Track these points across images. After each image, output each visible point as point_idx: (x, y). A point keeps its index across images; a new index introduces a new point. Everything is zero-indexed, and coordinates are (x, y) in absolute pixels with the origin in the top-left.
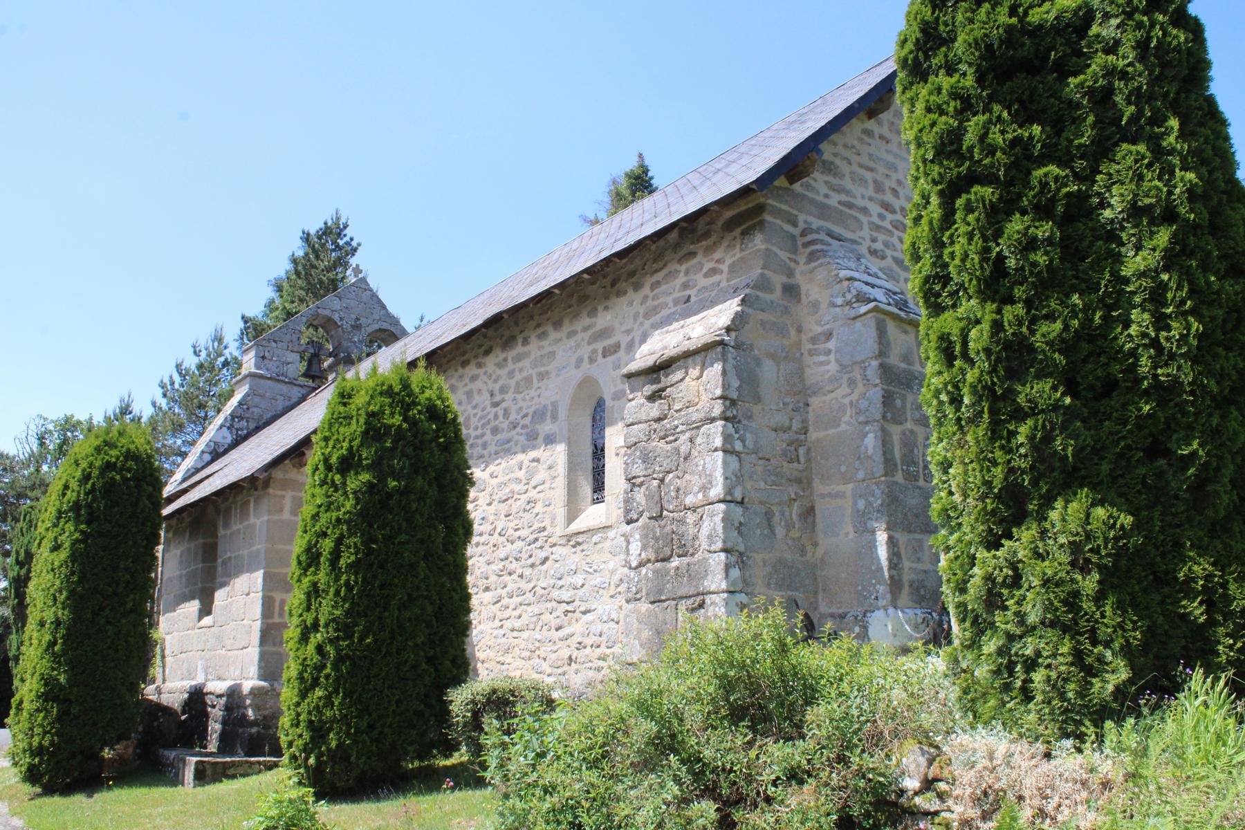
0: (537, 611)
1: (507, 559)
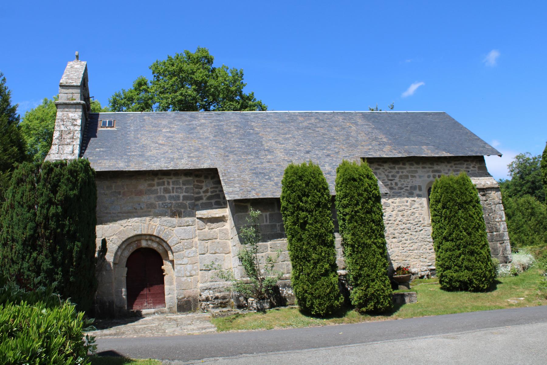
0: (420, 244)
1: (404, 229)
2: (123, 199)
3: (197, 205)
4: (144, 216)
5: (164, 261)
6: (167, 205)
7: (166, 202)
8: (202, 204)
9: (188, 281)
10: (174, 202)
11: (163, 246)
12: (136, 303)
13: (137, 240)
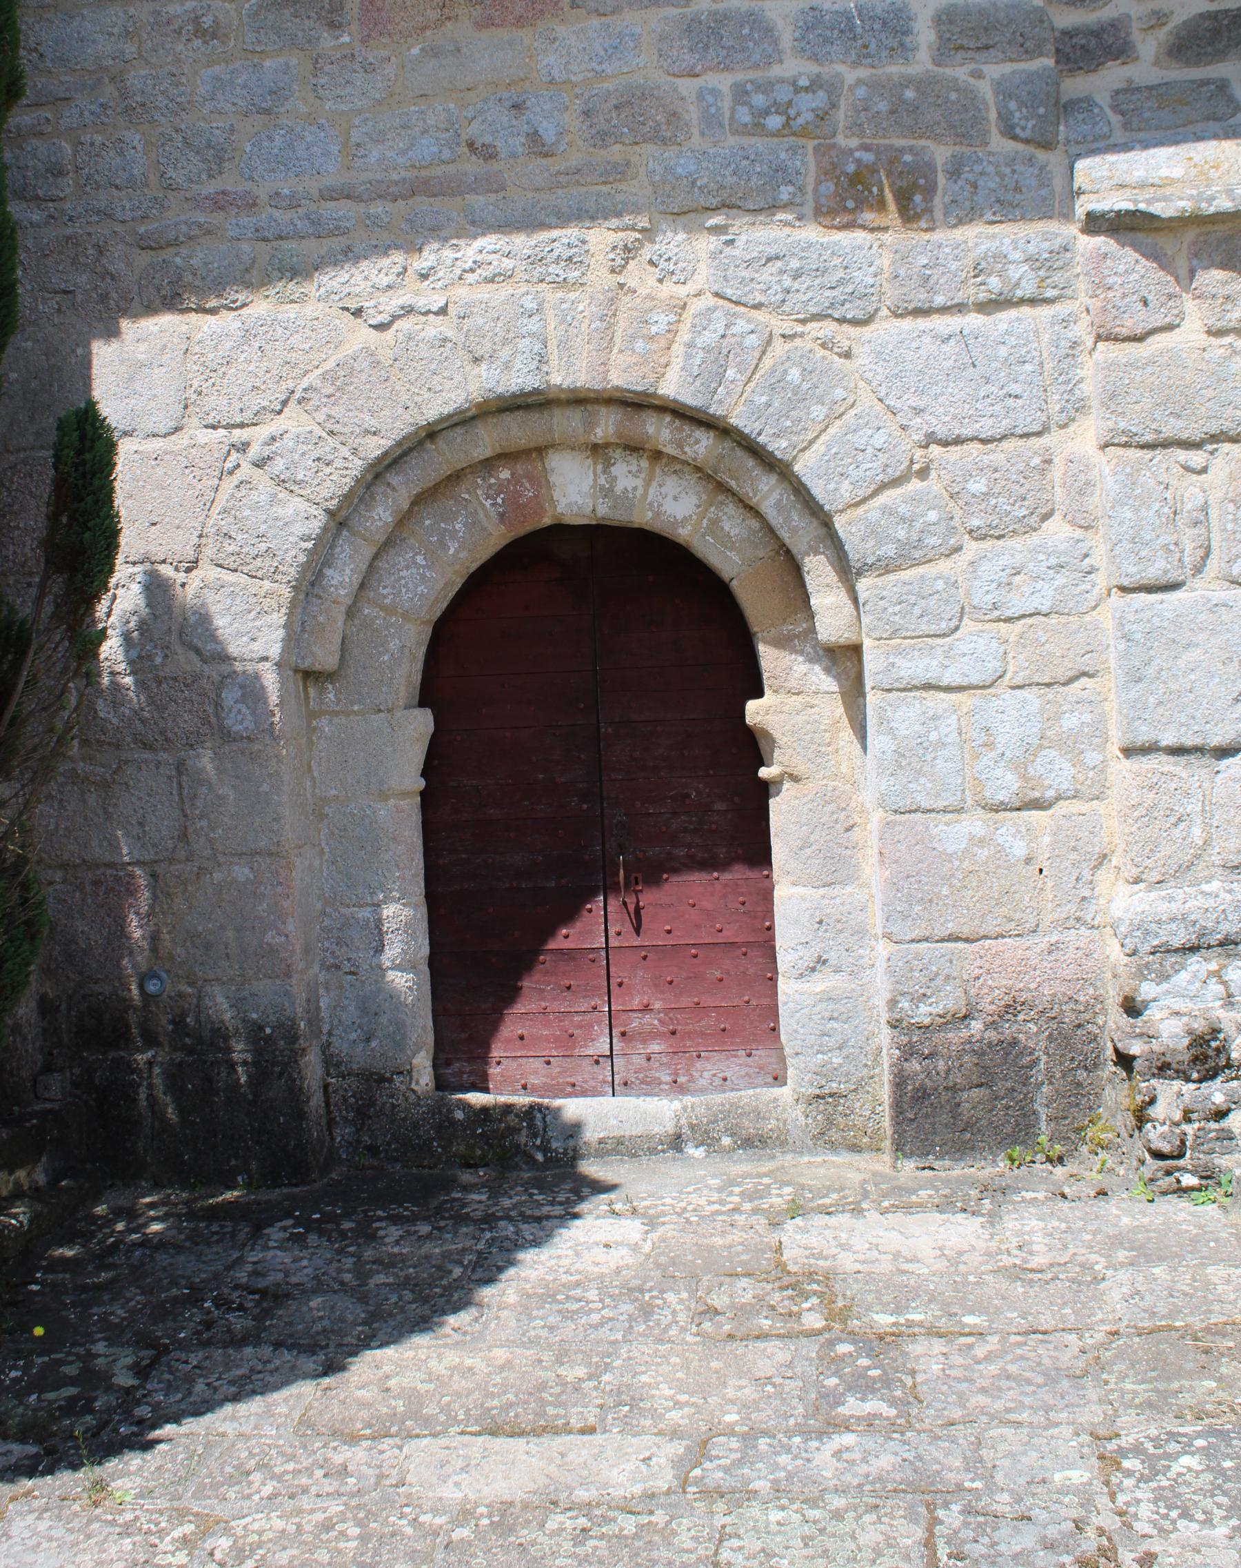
2: (368, 68)
3: (1083, 105)
4: (563, 218)
5: (762, 649)
6: (782, 109)
7: (776, 71)
8: (1124, 97)
9: (1000, 850)
10: (851, 75)
11: (753, 511)
12: (511, 1027)
13: (505, 457)
